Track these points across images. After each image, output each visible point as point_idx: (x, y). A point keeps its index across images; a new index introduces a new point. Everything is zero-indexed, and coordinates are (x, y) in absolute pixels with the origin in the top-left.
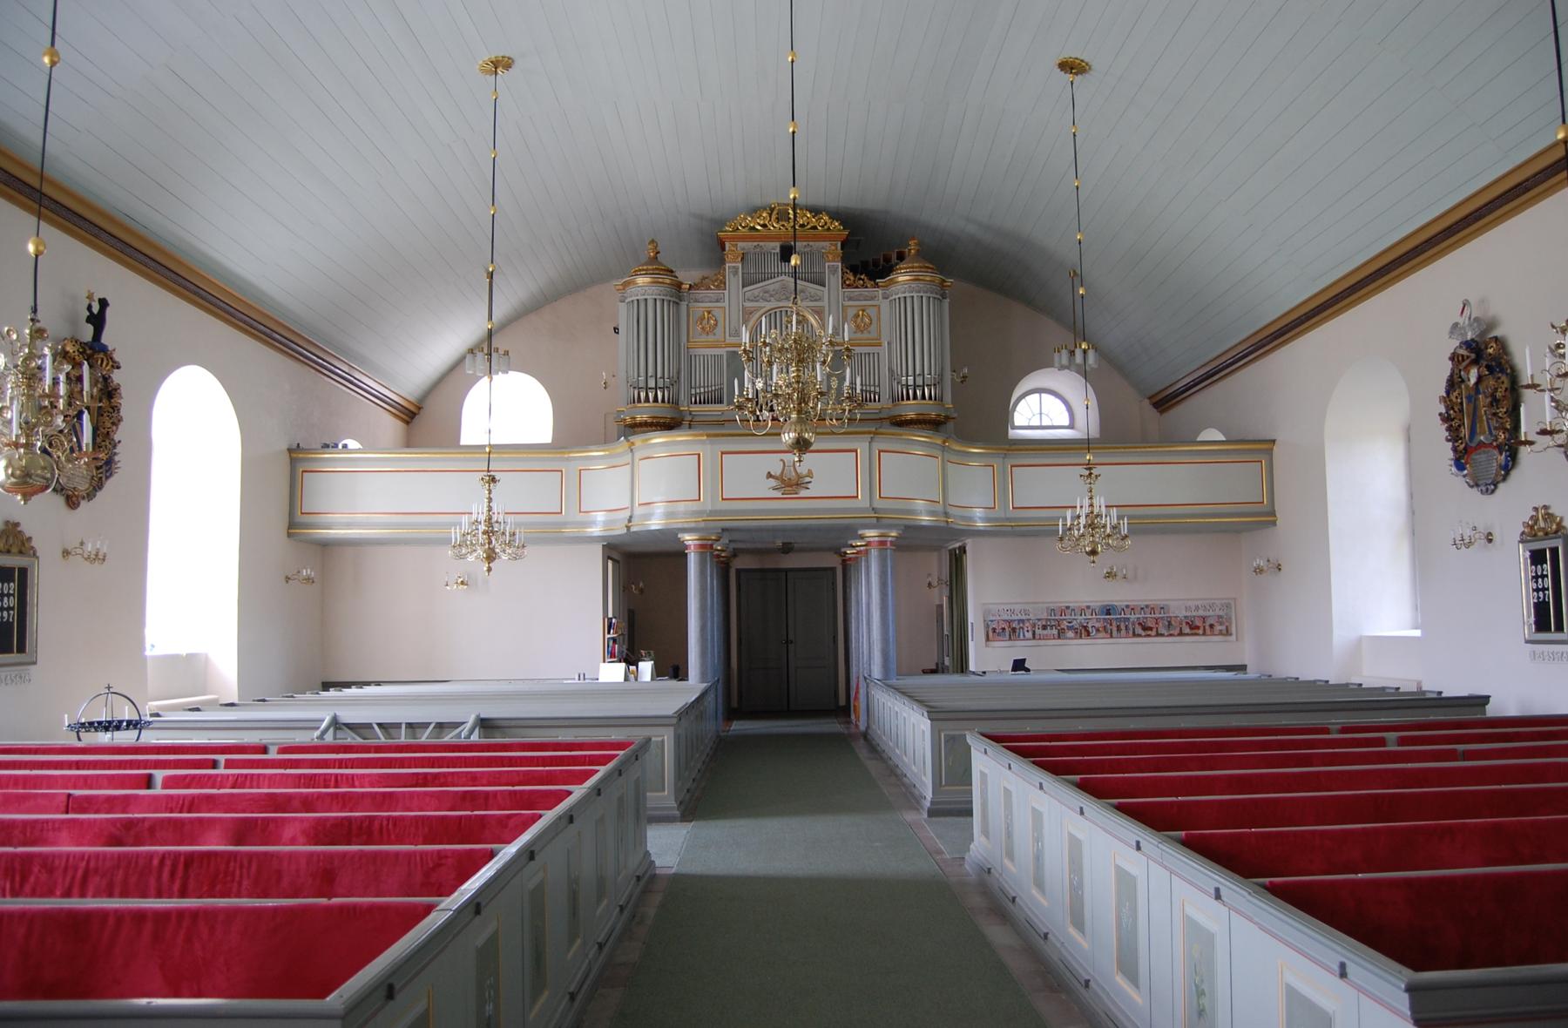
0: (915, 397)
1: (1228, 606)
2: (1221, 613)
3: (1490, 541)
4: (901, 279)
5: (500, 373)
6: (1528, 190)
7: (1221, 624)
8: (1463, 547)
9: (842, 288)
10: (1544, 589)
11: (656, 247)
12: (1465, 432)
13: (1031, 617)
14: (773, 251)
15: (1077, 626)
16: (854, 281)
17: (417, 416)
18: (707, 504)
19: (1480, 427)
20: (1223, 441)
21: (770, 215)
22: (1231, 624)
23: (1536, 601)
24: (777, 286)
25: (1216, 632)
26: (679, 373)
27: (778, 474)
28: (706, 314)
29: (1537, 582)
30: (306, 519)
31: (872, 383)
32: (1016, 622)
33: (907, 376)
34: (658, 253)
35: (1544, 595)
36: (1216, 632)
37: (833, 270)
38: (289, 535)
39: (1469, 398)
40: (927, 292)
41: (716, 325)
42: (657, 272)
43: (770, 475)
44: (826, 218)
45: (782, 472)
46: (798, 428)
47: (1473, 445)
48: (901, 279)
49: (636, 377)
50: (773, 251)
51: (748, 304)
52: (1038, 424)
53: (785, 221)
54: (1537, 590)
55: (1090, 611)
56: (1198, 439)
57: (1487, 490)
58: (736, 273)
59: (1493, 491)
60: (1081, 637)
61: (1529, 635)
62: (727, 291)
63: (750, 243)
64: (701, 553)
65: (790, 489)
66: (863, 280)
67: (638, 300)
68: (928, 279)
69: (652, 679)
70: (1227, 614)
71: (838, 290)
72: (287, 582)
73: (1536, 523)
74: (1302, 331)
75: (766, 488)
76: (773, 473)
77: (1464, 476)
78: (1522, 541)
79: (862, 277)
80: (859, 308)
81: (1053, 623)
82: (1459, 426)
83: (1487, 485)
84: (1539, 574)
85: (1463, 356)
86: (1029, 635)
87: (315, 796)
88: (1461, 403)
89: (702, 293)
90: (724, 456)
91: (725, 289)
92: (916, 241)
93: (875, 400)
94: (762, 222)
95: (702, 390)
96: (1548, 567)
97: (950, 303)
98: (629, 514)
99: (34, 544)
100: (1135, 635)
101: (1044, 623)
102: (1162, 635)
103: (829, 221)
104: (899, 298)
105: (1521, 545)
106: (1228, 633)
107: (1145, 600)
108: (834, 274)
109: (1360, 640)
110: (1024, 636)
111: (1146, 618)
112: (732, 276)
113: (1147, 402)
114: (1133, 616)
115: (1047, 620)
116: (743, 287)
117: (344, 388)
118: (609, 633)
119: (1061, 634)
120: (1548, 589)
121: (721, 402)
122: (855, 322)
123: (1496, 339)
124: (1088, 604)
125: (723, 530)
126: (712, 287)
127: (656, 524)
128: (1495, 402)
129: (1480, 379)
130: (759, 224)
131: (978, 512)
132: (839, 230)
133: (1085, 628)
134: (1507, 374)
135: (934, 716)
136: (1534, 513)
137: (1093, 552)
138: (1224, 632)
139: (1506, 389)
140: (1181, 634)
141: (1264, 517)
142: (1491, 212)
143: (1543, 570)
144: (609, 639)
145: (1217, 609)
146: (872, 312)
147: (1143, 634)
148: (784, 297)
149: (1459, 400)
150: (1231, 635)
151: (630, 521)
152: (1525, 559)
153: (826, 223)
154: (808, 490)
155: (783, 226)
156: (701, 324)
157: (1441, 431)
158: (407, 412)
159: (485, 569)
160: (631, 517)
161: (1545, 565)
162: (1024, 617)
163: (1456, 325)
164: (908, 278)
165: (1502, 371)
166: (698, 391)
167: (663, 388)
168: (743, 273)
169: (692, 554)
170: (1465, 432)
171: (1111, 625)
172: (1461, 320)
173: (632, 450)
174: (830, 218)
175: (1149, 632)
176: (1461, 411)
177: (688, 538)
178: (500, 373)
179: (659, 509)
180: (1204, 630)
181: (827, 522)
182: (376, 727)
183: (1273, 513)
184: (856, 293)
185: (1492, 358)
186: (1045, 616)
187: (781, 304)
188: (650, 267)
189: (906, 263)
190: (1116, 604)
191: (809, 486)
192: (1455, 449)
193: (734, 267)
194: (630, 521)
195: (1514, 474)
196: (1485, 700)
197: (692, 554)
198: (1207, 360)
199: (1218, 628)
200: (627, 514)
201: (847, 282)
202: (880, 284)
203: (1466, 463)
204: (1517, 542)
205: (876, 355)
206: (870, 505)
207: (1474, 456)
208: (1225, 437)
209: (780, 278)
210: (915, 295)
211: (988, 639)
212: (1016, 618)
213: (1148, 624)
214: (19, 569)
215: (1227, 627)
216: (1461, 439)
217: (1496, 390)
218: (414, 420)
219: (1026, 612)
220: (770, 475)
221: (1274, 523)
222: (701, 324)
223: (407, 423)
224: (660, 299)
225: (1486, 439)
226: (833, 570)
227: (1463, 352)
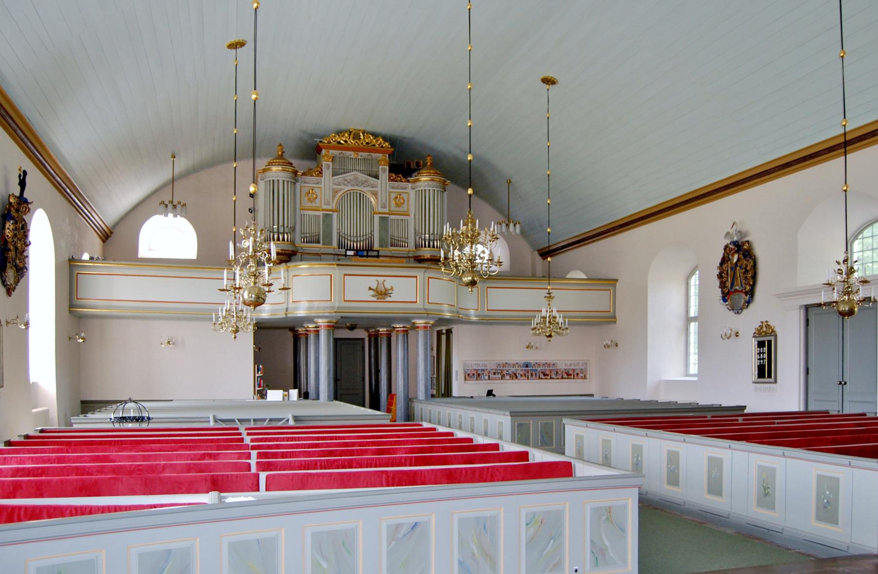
0: (429, 246)
1: (586, 364)
2: (582, 368)
3: (737, 336)
4: (423, 179)
5: (179, 216)
6: (770, 173)
7: (582, 373)
8: (726, 339)
9: (389, 181)
10: (763, 359)
11: (282, 149)
12: (729, 284)
13: (488, 368)
14: (350, 157)
15: (511, 373)
16: (395, 178)
17: (110, 238)
18: (337, 303)
19: (737, 282)
20: (586, 279)
22: (587, 373)
23: (759, 364)
25: (580, 377)
26: (295, 224)
28: (311, 191)
29: (760, 356)
30: (80, 302)
31: (404, 236)
32: (480, 371)
33: (425, 234)
34: (284, 152)
35: (763, 362)
36: (580, 377)
37: (384, 171)
38: (70, 312)
39: (731, 268)
41: (316, 198)
42: (285, 164)
43: (370, 289)
44: (381, 140)
46: (471, 275)
47: (732, 290)
48: (423, 179)
49: (272, 225)
51: (335, 187)
53: (358, 139)
54: (760, 359)
55: (518, 365)
56: (567, 277)
57: (738, 312)
58: (328, 168)
59: (740, 313)
60: (513, 379)
61: (755, 379)
63: (337, 151)
65: (381, 296)
66: (400, 177)
69: (298, 399)
70: (585, 368)
72: (70, 340)
73: (761, 329)
75: (368, 295)
76: (372, 287)
77: (727, 305)
78: (754, 337)
79: (400, 176)
80: (398, 193)
81: (499, 371)
82: (726, 281)
83: (738, 310)
84: (761, 352)
85: (732, 248)
86: (487, 377)
87: (30, 469)
88: (728, 271)
89: (308, 178)
91: (322, 177)
92: (430, 158)
93: (405, 246)
94: (344, 139)
95: (308, 235)
96: (766, 349)
97: (447, 194)
98: (286, 307)
100: (540, 378)
101: (494, 371)
102: (553, 378)
103: (382, 142)
104: (422, 190)
105: (753, 339)
106: (585, 378)
108: (384, 173)
109: (660, 382)
110: (484, 378)
111: (546, 369)
112: (326, 170)
113: (537, 252)
114: (539, 368)
115: (496, 370)
117: (86, 222)
118: (258, 373)
119: (503, 377)
120: (765, 359)
121: (319, 242)
122: (395, 201)
123: (748, 242)
124: (517, 362)
125: (341, 317)
126: (314, 175)
127: (301, 313)
128: (746, 271)
129: (739, 260)
130: (343, 140)
131: (446, 307)
132: (388, 148)
133: (515, 374)
134: (752, 259)
135: (513, 414)
136: (761, 324)
137: (550, 336)
138: (584, 377)
139: (752, 266)
140: (562, 378)
141: (610, 319)
142: (750, 181)
143: (763, 350)
144: (258, 377)
145: (581, 365)
146: (405, 196)
147: (544, 377)
149: (727, 269)
150: (587, 379)
152: (755, 345)
153: (381, 143)
154: (390, 298)
155: (357, 142)
156: (308, 196)
157: (717, 282)
158: (104, 233)
159: (233, 337)
161: (764, 348)
162: (484, 368)
163: (728, 233)
165: (750, 257)
166: (305, 235)
167: (284, 233)
168: (332, 168)
169: (322, 330)
170: (729, 284)
171: (528, 373)
172: (731, 231)
173: (288, 271)
175: (547, 377)
176: (727, 274)
177: (321, 321)
178: (179, 216)
179: (305, 305)
180: (574, 376)
181: (402, 315)
182: (237, 421)
183: (615, 317)
184: (396, 185)
185: (746, 251)
186: (495, 367)
188: (281, 161)
189: (425, 170)
190: (530, 362)
191: (391, 295)
192: (723, 293)
193: (327, 164)
194: (287, 310)
195: (751, 305)
196: (744, 407)
197: (322, 330)
198: (578, 234)
199: (580, 375)
200: (284, 306)
201: (391, 178)
203: (728, 299)
204: (751, 337)
205: (406, 221)
206: (424, 306)
207: (732, 296)
208: (586, 275)
209: (353, 173)
210: (431, 189)
211: (465, 379)
212: (480, 368)
213: (546, 373)
215: (585, 375)
216: (726, 287)
217: (747, 266)
218: (108, 241)
219: (486, 365)
220: (370, 289)
221: (615, 322)
222: (308, 196)
223: (104, 241)
225: (739, 288)
226: (363, 339)
227: (732, 246)
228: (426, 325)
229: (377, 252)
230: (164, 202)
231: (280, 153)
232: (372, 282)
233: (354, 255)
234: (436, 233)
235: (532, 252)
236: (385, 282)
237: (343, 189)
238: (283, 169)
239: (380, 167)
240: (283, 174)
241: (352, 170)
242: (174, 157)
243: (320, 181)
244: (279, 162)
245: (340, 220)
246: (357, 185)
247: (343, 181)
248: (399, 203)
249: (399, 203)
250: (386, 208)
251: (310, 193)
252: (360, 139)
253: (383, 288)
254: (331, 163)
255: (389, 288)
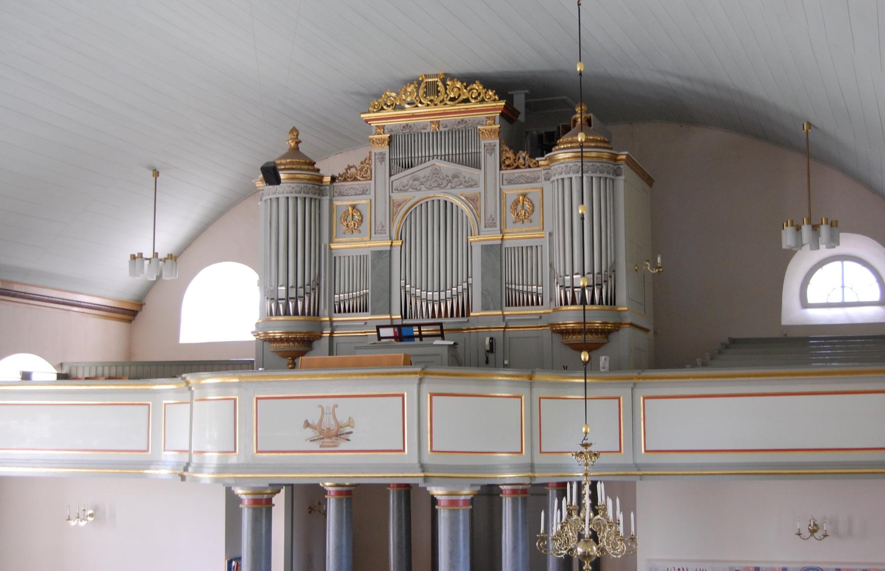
9: (501, 169)
14: (423, 131)
21: (418, 89)
24: (427, 172)
27: (316, 422)
28: (350, 209)
43: (307, 425)
45: (321, 421)
50: (423, 131)
52: (839, 300)
58: (383, 159)
62: (372, 182)
64: (254, 509)
67: (271, 199)
68: (594, 155)
75: (302, 438)
76: (310, 422)
90: (258, 401)
91: (371, 179)
97: (625, 180)
98: (187, 460)
104: (557, 180)
107: (836, 563)
116: (390, 175)
146: (535, 196)
148: (436, 184)
151: (186, 469)
153: (479, 94)
160: (188, 464)
164: (569, 155)
174: (484, 88)
184: (516, 175)
191: (350, 437)
197: (246, 509)
201: (507, 162)
209: (432, 162)
210: (573, 176)
214: (459, 317)
220: (307, 425)
224: (301, 198)
228: (454, 498)
229: (382, 335)
230: (141, 254)
231: (292, 144)
232: (312, 411)
233: (553, 312)
234: (596, 270)
236: (336, 409)
238: (292, 176)
239: (544, 143)
240: (293, 185)
241: (433, 156)
242: (156, 174)
243: (368, 187)
244: (597, 141)
247: (411, 182)
250: (496, 226)
251: (519, 201)
252: (438, 92)
253: (333, 422)
255: (345, 421)
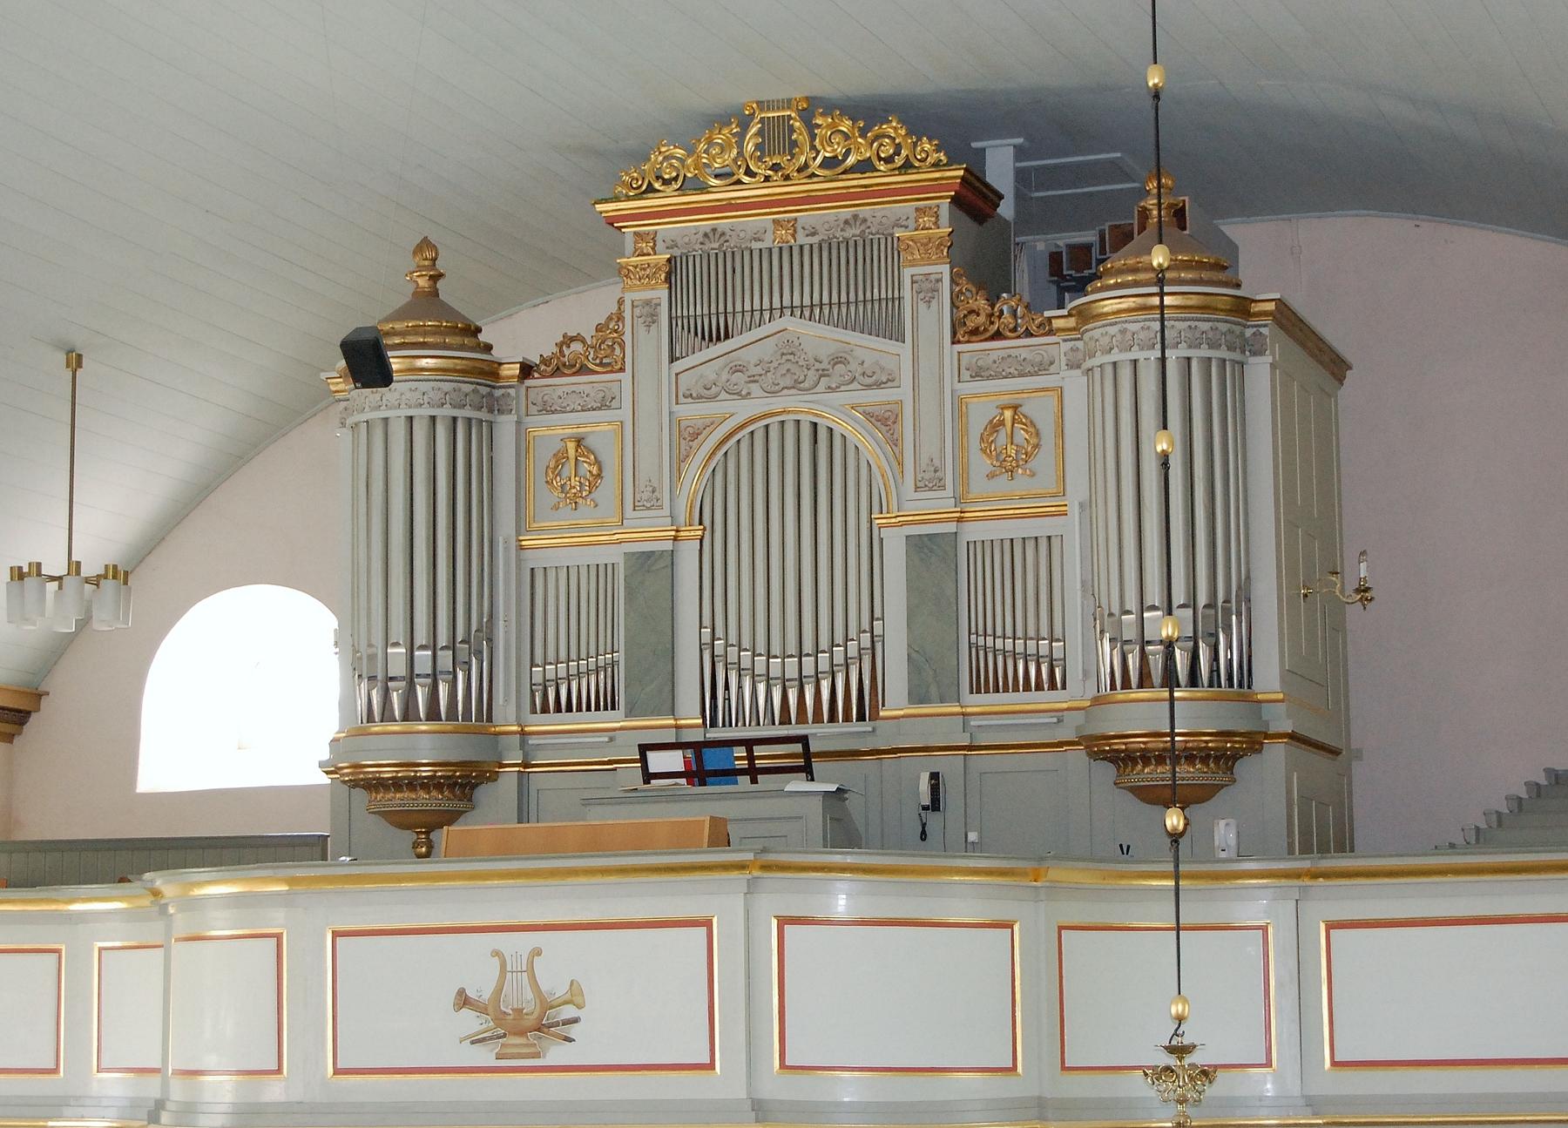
4: (1110, 306)
14: (756, 245)
27: (486, 995)
40: (1199, 346)
43: (463, 1001)
45: (499, 990)
48: (1110, 306)
71: (941, 347)
74: (905, 854)
76: (471, 993)
91: (622, 370)
99: (325, 755)
112: (641, 330)
116: (673, 359)
146: (1040, 410)
184: (994, 355)
187: (776, 404)
191: (573, 1032)
193: (648, 303)
202: (1057, 324)
206: (749, 1093)
209: (767, 329)
220: (463, 1001)
235: (925, 808)
237: (712, 425)
242: (75, 361)
245: (713, 583)
246: (796, 385)
247: (725, 376)
248: (1012, 451)
249: (1012, 451)
253: (529, 995)
254: (662, 293)
255: (561, 990)
